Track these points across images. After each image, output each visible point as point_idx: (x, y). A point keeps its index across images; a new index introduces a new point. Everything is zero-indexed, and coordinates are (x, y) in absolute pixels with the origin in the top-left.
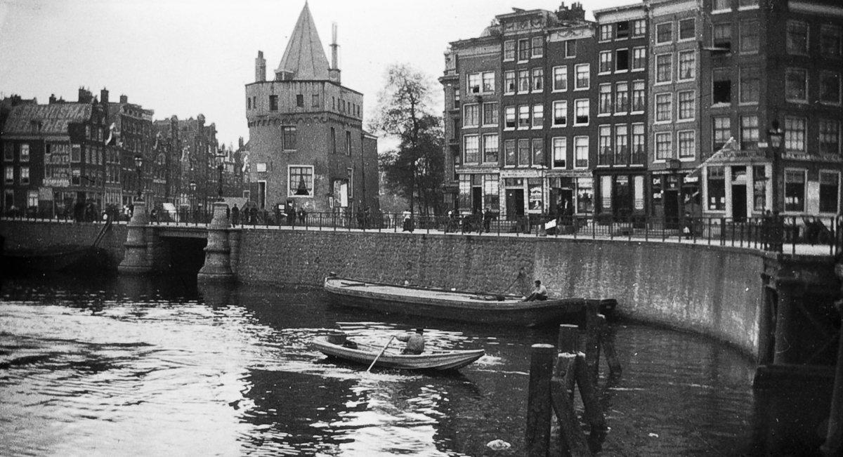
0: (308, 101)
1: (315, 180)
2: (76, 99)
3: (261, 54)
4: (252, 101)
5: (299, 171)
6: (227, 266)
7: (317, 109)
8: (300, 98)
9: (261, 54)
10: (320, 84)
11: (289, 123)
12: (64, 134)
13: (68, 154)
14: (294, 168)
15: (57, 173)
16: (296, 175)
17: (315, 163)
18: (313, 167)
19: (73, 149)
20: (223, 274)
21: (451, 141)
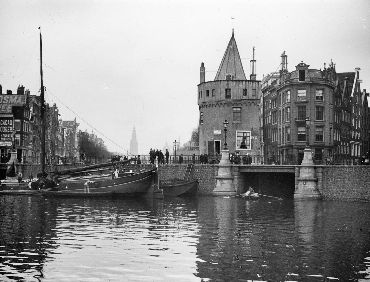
0: (250, 93)
1: (252, 140)
2: (6, 93)
3: (203, 64)
4: (200, 93)
5: (242, 134)
6: (317, 189)
7: (254, 98)
8: (245, 90)
9: (203, 64)
10: (256, 83)
11: (237, 105)
12: (10, 113)
13: (12, 126)
14: (239, 132)
15: (4, 137)
16: (240, 136)
17: (252, 130)
18: (251, 132)
19: (15, 122)
20: (316, 195)
21: (296, 119)
